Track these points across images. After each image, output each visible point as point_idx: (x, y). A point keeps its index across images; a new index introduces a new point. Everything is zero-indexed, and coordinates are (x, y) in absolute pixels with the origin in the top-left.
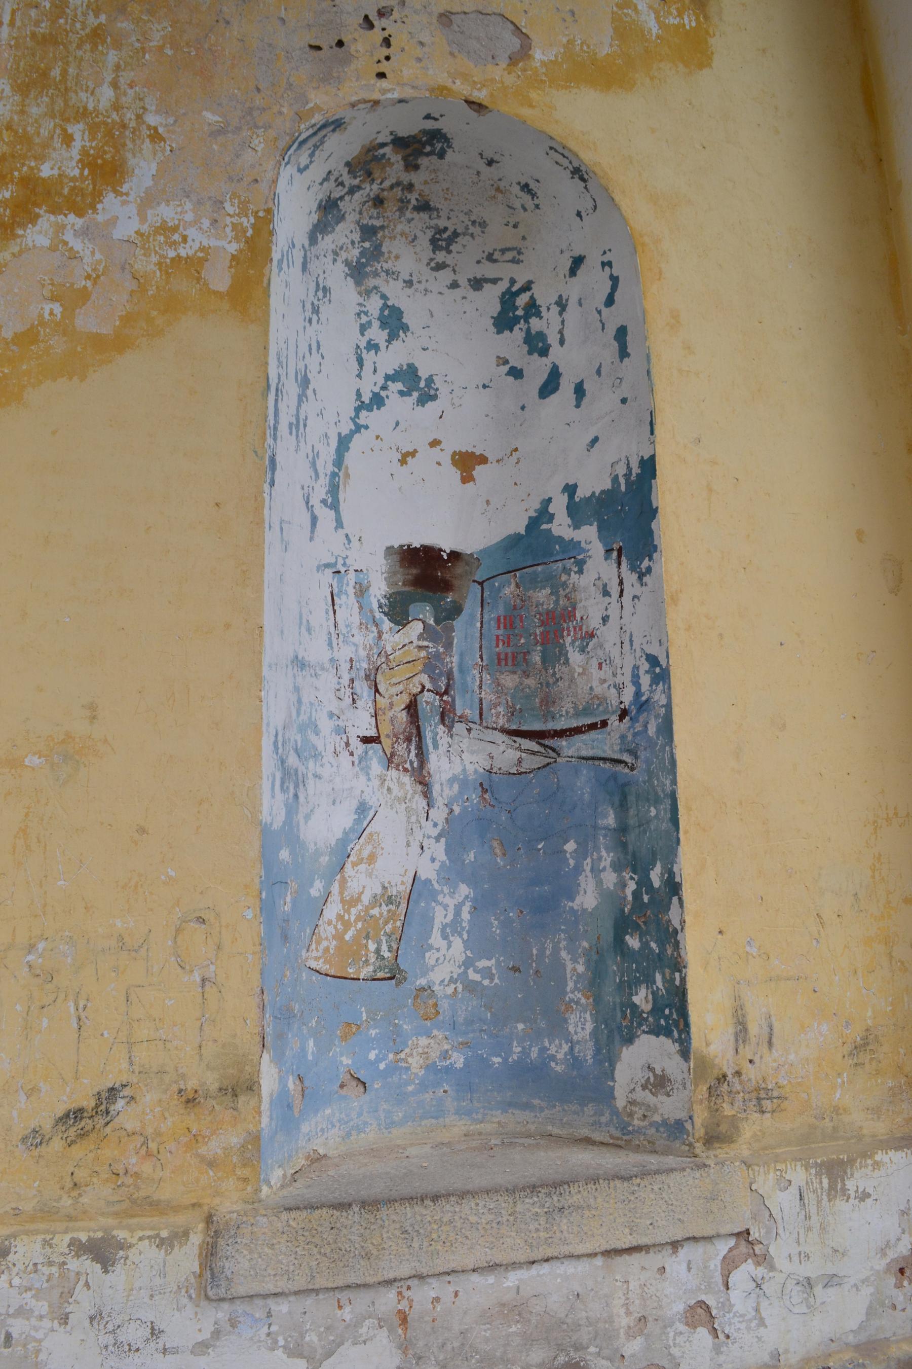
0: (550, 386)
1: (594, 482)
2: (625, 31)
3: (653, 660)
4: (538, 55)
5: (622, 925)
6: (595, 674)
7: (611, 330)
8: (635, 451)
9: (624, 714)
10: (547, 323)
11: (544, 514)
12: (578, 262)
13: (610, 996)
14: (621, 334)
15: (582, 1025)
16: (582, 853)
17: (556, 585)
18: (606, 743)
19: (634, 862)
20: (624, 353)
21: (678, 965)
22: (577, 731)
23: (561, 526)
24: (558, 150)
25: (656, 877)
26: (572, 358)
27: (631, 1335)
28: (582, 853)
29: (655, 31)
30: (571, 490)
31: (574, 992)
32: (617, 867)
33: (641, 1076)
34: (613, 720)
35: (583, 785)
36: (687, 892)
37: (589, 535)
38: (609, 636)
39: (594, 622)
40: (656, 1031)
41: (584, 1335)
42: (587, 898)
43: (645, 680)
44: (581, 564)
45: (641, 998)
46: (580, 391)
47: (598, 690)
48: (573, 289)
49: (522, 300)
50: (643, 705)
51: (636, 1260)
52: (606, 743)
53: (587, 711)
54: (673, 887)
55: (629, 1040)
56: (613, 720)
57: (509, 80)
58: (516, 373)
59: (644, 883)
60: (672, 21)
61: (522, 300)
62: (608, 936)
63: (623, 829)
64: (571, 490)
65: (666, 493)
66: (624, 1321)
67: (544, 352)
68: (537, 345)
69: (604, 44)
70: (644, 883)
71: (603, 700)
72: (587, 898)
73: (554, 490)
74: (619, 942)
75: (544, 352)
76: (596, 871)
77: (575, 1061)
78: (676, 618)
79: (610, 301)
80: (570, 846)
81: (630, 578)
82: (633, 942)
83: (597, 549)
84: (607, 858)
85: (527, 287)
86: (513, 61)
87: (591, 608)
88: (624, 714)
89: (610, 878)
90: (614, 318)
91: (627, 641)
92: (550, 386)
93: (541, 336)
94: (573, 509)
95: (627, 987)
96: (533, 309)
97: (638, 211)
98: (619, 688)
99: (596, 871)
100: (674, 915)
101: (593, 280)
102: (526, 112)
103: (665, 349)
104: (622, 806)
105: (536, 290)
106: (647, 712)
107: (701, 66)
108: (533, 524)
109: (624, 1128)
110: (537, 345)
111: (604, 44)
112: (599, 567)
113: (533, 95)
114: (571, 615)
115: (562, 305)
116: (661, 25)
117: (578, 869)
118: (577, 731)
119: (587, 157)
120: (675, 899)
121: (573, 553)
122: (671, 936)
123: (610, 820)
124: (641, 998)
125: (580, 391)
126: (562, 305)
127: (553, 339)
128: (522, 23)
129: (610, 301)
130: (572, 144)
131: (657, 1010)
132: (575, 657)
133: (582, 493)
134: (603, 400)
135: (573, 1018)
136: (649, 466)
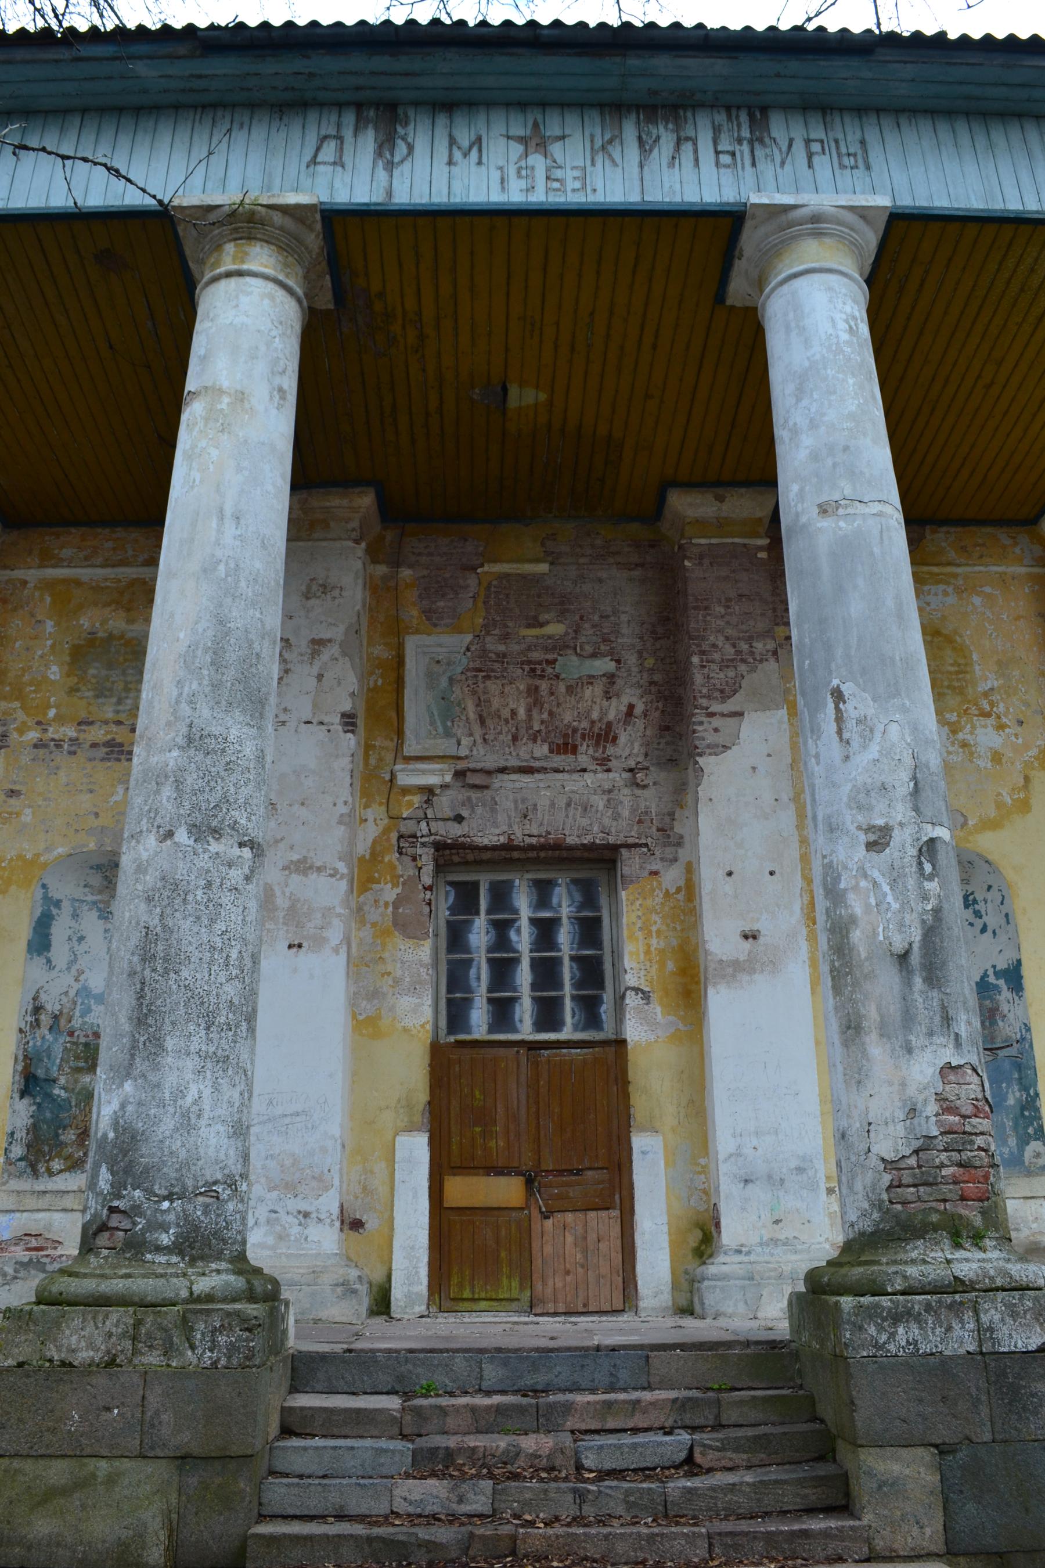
0: (984, 930)
1: (1002, 965)
2: (999, 805)
3: (1025, 1025)
4: (970, 823)
5: (1023, 1108)
6: (1008, 1029)
7: (1004, 913)
8: (1015, 957)
9: (1018, 1042)
10: (981, 907)
11: (985, 975)
12: (990, 887)
13: (1021, 1132)
14: (1007, 915)
15: (1012, 1142)
16: (1008, 1087)
17: (992, 1000)
18: (1013, 1051)
19: (1025, 1088)
20: (1008, 923)
21: (1040, 1118)
22: (1003, 1048)
23: (992, 979)
24: (980, 856)
25: (1032, 1092)
26: (992, 920)
27: (1033, 1222)
28: (1008, 1087)
29: (1010, 802)
30: (994, 967)
31: (1009, 1132)
32: (1020, 1090)
33: (1032, 1154)
34: (1015, 1044)
35: (1007, 1065)
36: (1041, 1096)
37: (1001, 982)
38: (1011, 1016)
39: (1006, 1012)
40: (1036, 1140)
41: (1019, 1221)
42: (1011, 1101)
43: (1024, 1031)
44: (1000, 992)
45: (1030, 1130)
46: (994, 932)
47: (1009, 1034)
48: (989, 896)
49: (971, 898)
50: (1023, 1039)
51: (1032, 1201)
52: (1013, 1051)
53: (1006, 1041)
54: (1037, 1095)
55: (1028, 1144)
56: (1015, 1044)
57: (962, 834)
58: (971, 924)
59: (1028, 1094)
60: (1016, 797)
61: (971, 898)
62: (1018, 1111)
63: (1020, 1079)
64: (994, 967)
65: (1025, 971)
66: (1031, 1218)
67: (981, 917)
68: (978, 914)
69: (992, 813)
70: (1028, 1094)
71: (1011, 1037)
72: (1011, 1101)
73: (988, 966)
74: (1022, 1115)
75: (981, 917)
76: (1013, 1092)
77: (1011, 1153)
78: (1032, 1011)
79: (1002, 903)
80: (1004, 1085)
81: (1016, 998)
82: (1027, 1113)
83: (1005, 987)
84: (1016, 1088)
85: (972, 893)
86: (962, 827)
87: (1004, 1007)
88: (1018, 1042)
89: (1018, 1094)
90: (1004, 909)
91: (1017, 1018)
92: (984, 930)
93: (979, 911)
94: (995, 973)
95: (1026, 1127)
96: (975, 901)
97: (1010, 874)
98: (1016, 1034)
99: (1013, 1092)
100: (1038, 1103)
101: (994, 895)
102: (968, 845)
103: (1022, 922)
104: (1020, 1071)
105: (976, 895)
106: (1025, 1041)
107: (1028, 812)
108: (982, 978)
109: (1028, 1171)
110: (978, 914)
111: (992, 813)
112: (1006, 994)
113: (970, 838)
114: (998, 1010)
115: (986, 901)
116: (1012, 799)
117: (1007, 1092)
118: (1003, 1048)
119: (990, 858)
120: (300, 291)
121: (996, 987)
122: (1037, 1110)
123: (1016, 1076)
124: (1030, 1130)
125: (994, 932)
126: (986, 901)
127: (983, 913)
128: (964, 811)
129: (1002, 903)
130: (984, 854)
131: (1035, 1133)
132: (1000, 1023)
133: (998, 968)
134: (1002, 937)
135: (1010, 1140)
136: (1019, 962)
